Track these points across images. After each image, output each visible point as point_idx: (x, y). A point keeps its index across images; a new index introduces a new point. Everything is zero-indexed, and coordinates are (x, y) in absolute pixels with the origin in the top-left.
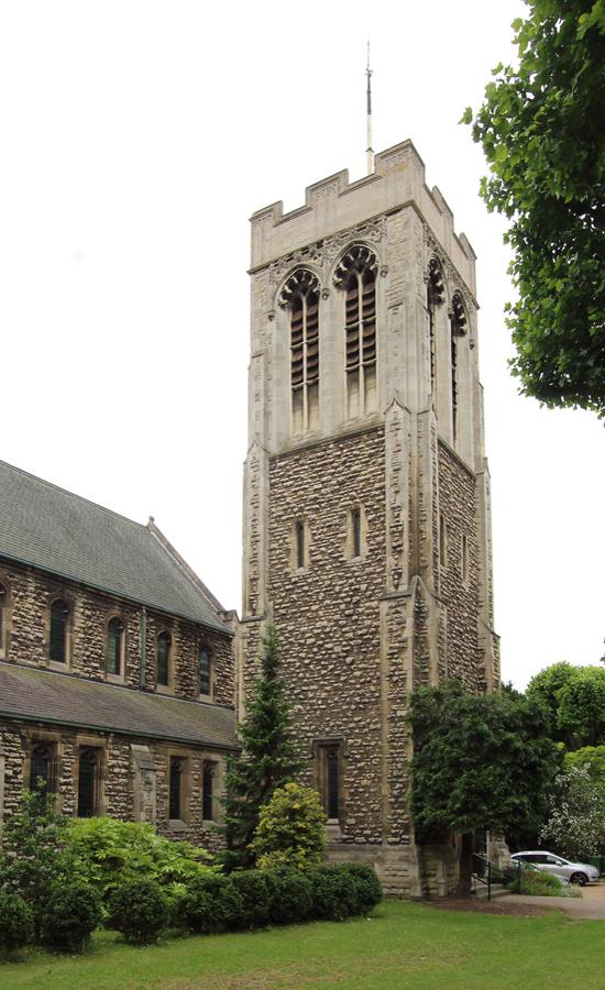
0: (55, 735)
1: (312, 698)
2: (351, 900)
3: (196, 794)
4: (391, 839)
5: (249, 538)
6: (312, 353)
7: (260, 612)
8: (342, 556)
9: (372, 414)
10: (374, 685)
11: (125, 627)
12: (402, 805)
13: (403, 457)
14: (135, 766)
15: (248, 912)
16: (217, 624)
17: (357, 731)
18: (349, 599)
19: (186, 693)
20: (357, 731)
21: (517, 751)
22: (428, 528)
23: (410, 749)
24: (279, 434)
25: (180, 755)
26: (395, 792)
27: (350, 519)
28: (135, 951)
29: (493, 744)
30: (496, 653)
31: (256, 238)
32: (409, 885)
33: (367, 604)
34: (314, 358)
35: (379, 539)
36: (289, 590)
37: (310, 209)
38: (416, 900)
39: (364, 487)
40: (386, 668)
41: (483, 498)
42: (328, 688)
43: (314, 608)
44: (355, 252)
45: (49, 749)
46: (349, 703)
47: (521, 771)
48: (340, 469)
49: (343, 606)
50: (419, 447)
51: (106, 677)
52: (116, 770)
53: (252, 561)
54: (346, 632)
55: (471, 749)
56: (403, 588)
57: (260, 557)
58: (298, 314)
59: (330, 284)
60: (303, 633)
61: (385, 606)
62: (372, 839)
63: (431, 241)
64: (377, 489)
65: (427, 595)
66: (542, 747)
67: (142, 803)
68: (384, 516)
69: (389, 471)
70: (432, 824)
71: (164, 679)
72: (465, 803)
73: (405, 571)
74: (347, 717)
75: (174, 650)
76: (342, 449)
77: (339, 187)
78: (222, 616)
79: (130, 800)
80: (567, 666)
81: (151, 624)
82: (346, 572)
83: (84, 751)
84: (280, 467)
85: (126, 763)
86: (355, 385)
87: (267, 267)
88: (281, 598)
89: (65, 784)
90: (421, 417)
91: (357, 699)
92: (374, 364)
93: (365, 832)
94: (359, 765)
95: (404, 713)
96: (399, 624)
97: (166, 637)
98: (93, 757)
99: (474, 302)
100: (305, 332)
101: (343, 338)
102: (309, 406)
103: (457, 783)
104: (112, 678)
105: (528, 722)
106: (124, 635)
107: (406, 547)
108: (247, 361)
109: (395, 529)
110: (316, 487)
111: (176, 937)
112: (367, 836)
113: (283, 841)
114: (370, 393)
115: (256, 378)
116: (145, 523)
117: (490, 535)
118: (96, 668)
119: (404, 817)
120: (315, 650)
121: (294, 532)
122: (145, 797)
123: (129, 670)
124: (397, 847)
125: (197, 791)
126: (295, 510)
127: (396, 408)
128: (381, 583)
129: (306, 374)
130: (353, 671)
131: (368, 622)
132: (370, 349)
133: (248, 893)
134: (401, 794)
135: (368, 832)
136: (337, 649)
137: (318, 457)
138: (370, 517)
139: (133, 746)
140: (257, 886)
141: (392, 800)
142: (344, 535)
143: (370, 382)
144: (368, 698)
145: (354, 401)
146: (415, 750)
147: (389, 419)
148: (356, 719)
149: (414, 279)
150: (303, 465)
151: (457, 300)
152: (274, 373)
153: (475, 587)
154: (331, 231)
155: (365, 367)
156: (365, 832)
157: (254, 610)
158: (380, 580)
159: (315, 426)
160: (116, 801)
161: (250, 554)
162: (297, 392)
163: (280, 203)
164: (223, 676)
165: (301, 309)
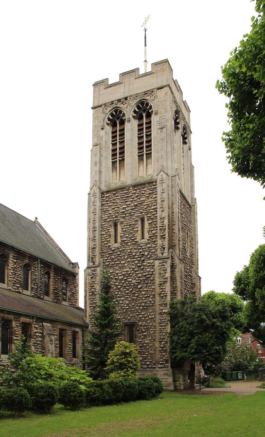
0: (11, 317)
1: (121, 304)
2: (147, 392)
3: (70, 346)
4: (160, 366)
5: (91, 228)
6: (122, 146)
7: (97, 263)
8: (136, 239)
9: (150, 175)
10: (151, 298)
11: (31, 268)
12: (165, 351)
13: (165, 195)
14: (45, 333)
15: (114, 397)
16: (69, 268)
17: (143, 319)
18: (139, 259)
19: (57, 300)
20: (143, 319)
21: (218, 326)
22: (176, 228)
23: (169, 326)
24: (106, 181)
25: (63, 328)
26: (162, 346)
27: (140, 222)
28: (73, 413)
29: (208, 324)
30: (200, 285)
31: (96, 93)
32: (169, 385)
33: (148, 261)
34: (122, 148)
35: (154, 232)
36: (110, 253)
37: (121, 83)
38: (171, 391)
39: (147, 208)
40: (158, 290)
41: (194, 216)
42: (129, 299)
43: (122, 262)
44: (142, 103)
45: (9, 324)
46: (139, 306)
47: (219, 335)
48: (136, 199)
49: (136, 262)
50: (172, 192)
51: (22, 291)
52: (37, 334)
53: (92, 239)
54: (138, 274)
55: (198, 326)
56: (165, 255)
57: (97, 238)
58: (115, 128)
59: (133, 117)
60: (117, 274)
61: (157, 263)
62: (150, 366)
63: (175, 102)
64: (153, 209)
65: (176, 258)
66: (228, 325)
67: (49, 349)
68: (156, 221)
69: (159, 201)
70: (181, 359)
71: (47, 294)
72: (196, 349)
73: (166, 247)
74: (139, 312)
75: (51, 280)
76: (136, 190)
77: (135, 75)
78: (71, 265)
79: (43, 348)
80: (214, 292)
81: (42, 267)
82: (138, 246)
83: (24, 325)
84: (106, 197)
85: (41, 331)
86: (142, 162)
87: (101, 106)
88: (106, 257)
89: (16, 340)
90: (173, 178)
91: (143, 304)
92: (151, 153)
93: (147, 363)
94: (144, 334)
95: (166, 311)
96: (164, 270)
97: (48, 274)
98: (27, 328)
99: (190, 130)
100: (118, 136)
101: (136, 141)
102: (120, 170)
103: (193, 340)
104: (25, 292)
105: (222, 314)
106: (30, 272)
107: (167, 236)
108: (91, 147)
109: (162, 228)
110: (123, 207)
111: (85, 407)
112: (148, 365)
113: (121, 366)
114: (149, 166)
115: (96, 155)
116: (33, 220)
117: (197, 233)
118: (18, 287)
119: (166, 356)
120: (123, 281)
121: (113, 227)
122: (50, 347)
123: (32, 288)
124: (162, 369)
125: (70, 345)
126: (113, 217)
127: (162, 173)
128: (154, 252)
129: (118, 155)
130: (141, 292)
131: (148, 270)
132: (149, 147)
133: (114, 388)
134: (165, 347)
135: (149, 363)
136: (133, 281)
137: (125, 193)
138: (149, 222)
139: (44, 323)
140: (117, 385)
141: (160, 349)
142: (137, 229)
143: (149, 161)
144: (148, 304)
145: (141, 169)
146: (171, 328)
147: (159, 178)
148: (143, 313)
149: (170, 117)
150: (117, 196)
151: (184, 129)
152: (104, 153)
153: (191, 256)
154: (131, 93)
155: (147, 154)
156: (147, 363)
157: (94, 262)
158: (154, 251)
159: (123, 179)
160: (37, 348)
161: (92, 236)
162: (114, 163)
163: (107, 79)
164: (73, 293)
165: (116, 126)
